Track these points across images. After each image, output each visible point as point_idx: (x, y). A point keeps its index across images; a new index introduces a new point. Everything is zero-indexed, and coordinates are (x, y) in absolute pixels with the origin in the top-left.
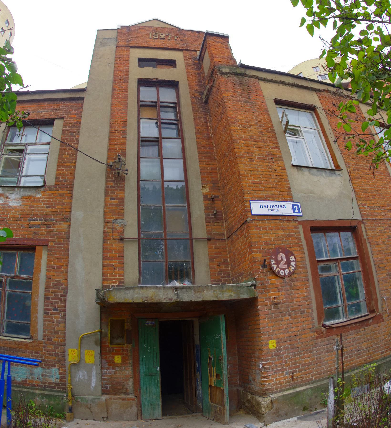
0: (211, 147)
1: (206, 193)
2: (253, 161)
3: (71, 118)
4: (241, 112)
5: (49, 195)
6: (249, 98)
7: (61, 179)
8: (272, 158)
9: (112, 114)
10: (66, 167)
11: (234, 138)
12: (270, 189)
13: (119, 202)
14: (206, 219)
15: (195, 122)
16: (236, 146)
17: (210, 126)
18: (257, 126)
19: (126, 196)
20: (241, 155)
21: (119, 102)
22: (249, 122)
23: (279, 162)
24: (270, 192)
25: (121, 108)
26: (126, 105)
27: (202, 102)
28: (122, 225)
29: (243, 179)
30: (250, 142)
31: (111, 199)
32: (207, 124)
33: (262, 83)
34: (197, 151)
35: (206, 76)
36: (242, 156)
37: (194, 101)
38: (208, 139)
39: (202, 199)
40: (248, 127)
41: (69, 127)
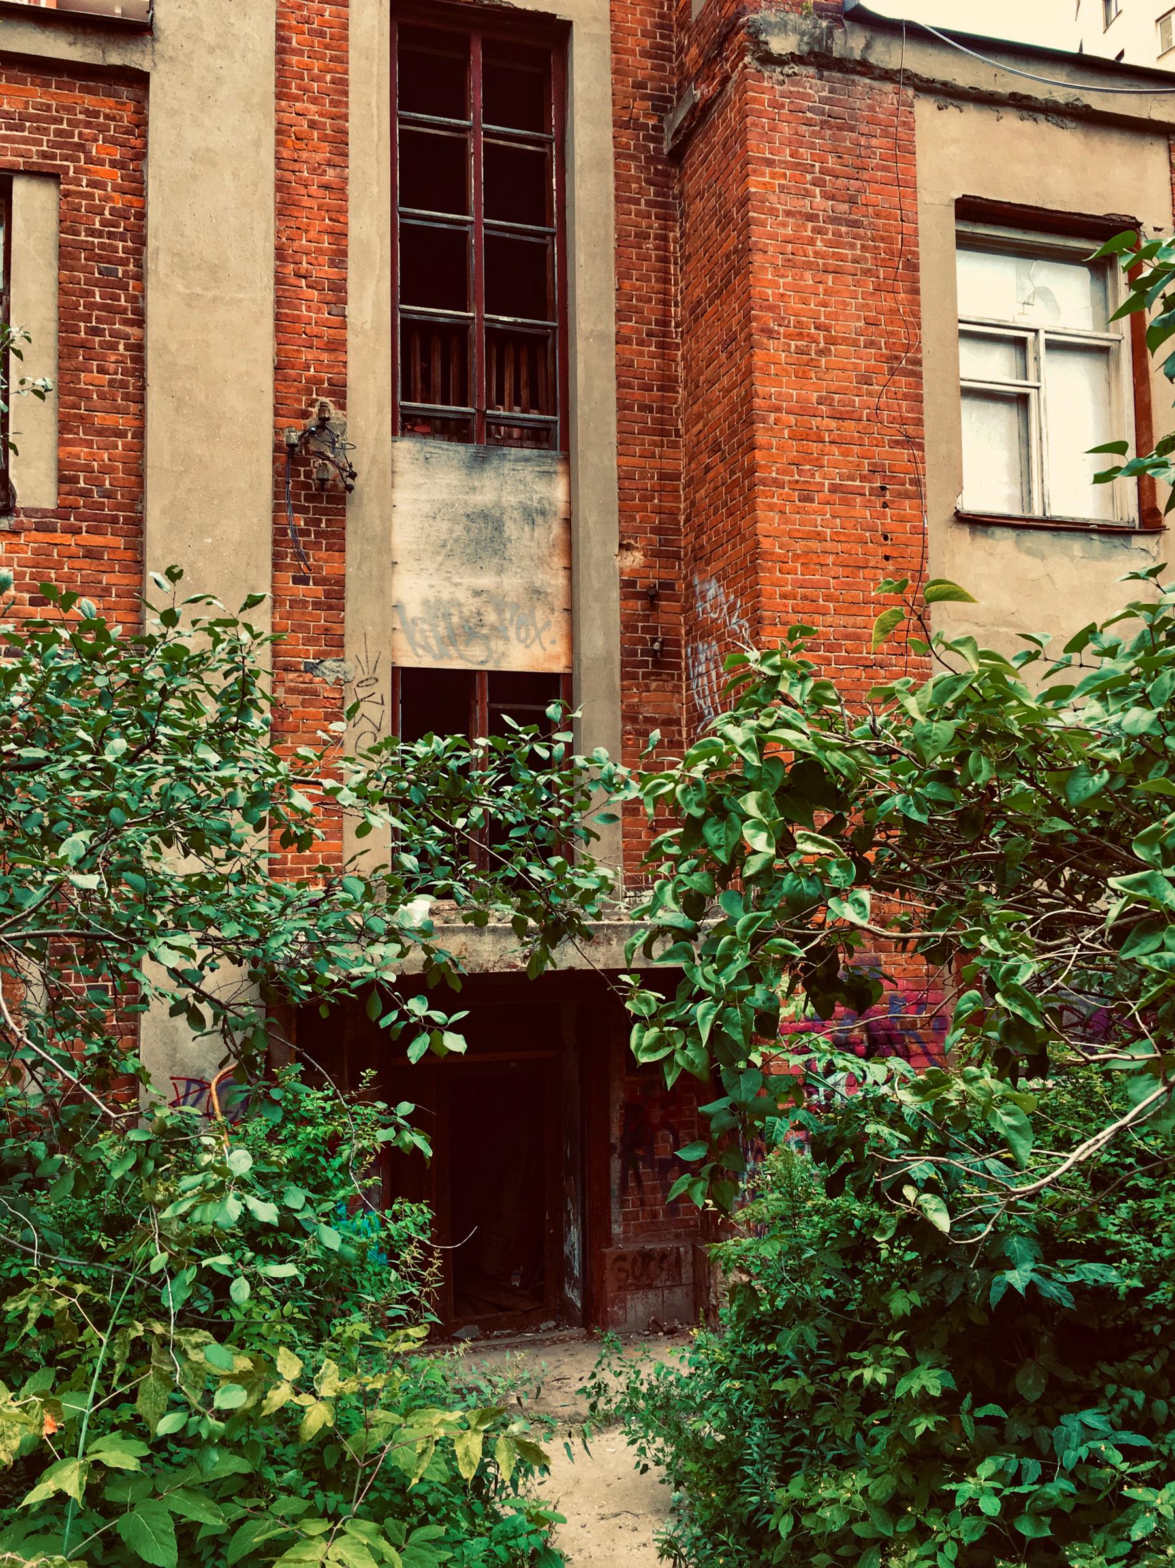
0: (668, 384)
1: (633, 570)
2: (812, 501)
3: (92, 184)
4: (808, 275)
5: (36, 552)
6: (852, 201)
7: (82, 484)
8: (883, 488)
9: (281, 186)
10: (100, 432)
11: (757, 401)
12: (854, 609)
13: (327, 594)
14: (623, 664)
15: (619, 255)
16: (761, 438)
17: (676, 284)
18: (855, 343)
19: (350, 571)
20: (774, 475)
21: (313, 125)
22: (827, 329)
23: (907, 503)
24: (851, 620)
25: (319, 157)
26: (339, 142)
27: (658, 150)
28: (338, 679)
29: (764, 569)
30: (815, 422)
31: (297, 580)
32: (666, 271)
33: (925, 109)
34: (614, 396)
35: (693, 19)
36: (775, 481)
37: (627, 145)
38: (662, 346)
39: (615, 594)
40: (820, 352)
41: (92, 232)
